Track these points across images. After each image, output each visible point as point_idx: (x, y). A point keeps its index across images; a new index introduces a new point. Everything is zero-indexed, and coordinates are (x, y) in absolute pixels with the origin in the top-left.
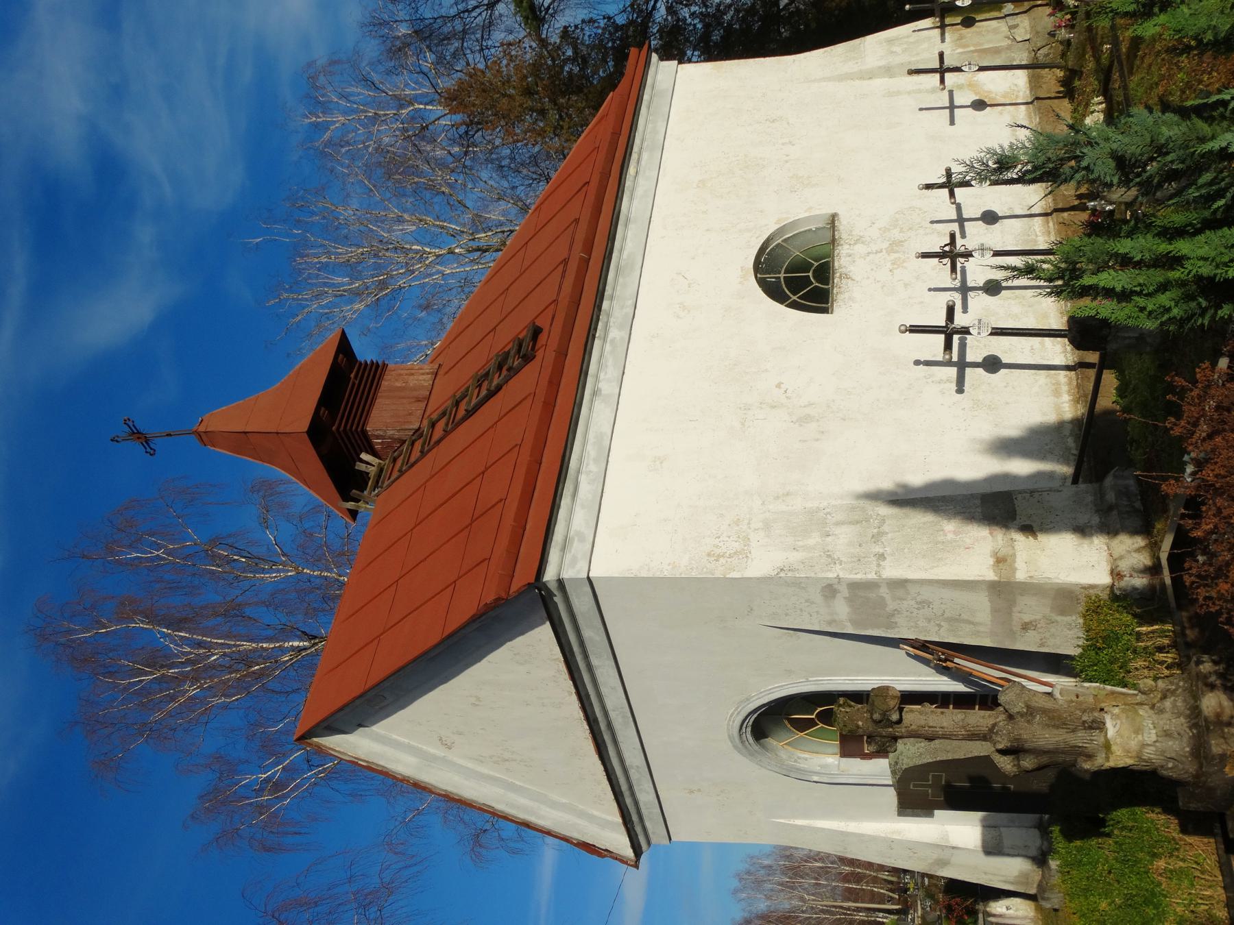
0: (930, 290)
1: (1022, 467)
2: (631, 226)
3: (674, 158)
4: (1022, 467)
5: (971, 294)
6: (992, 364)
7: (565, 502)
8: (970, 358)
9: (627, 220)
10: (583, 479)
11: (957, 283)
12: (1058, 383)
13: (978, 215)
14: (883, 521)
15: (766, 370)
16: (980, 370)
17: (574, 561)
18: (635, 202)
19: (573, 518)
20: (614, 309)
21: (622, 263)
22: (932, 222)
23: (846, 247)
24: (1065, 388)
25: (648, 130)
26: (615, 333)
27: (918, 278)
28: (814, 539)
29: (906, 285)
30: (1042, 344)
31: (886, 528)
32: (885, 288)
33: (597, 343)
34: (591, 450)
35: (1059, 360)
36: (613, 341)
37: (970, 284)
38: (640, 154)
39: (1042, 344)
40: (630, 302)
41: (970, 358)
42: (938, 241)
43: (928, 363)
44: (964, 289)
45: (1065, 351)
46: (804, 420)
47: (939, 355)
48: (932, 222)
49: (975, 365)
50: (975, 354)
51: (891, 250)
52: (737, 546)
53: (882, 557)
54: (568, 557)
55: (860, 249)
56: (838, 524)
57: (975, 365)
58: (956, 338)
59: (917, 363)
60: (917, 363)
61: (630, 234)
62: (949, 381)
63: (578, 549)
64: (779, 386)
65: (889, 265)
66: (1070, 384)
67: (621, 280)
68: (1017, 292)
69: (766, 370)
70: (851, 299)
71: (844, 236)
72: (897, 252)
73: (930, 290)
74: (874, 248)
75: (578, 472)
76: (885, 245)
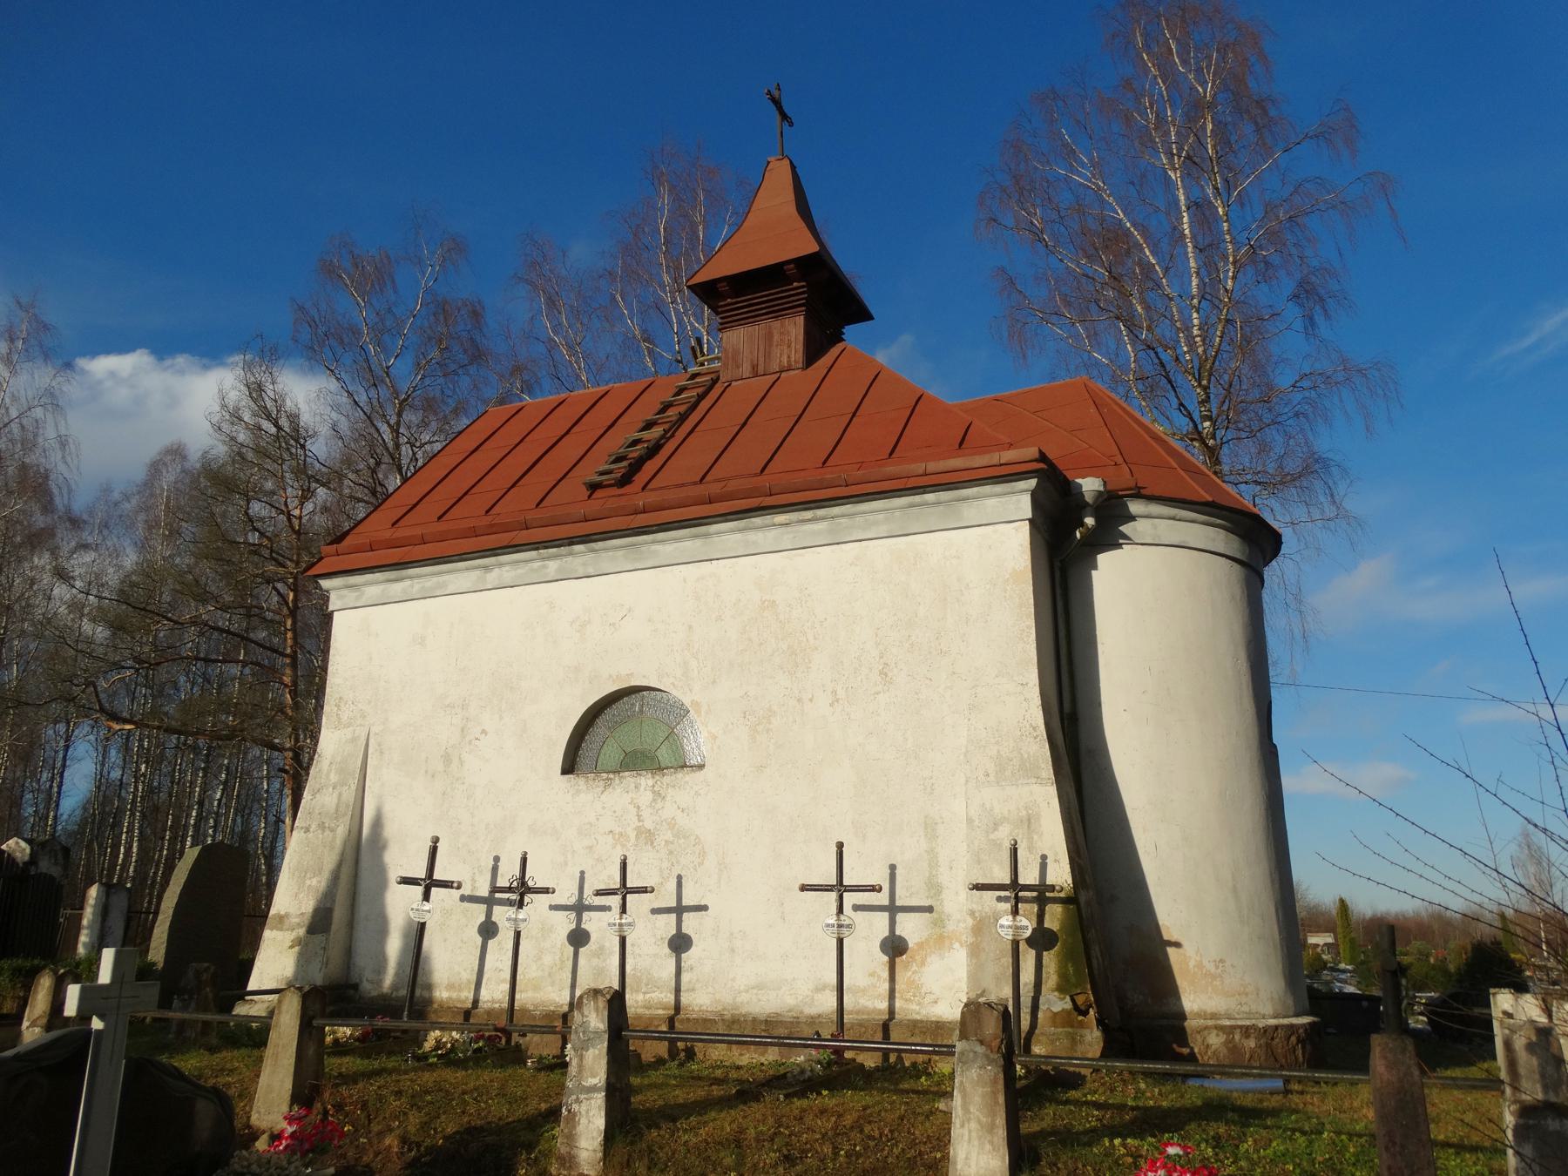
0: (582, 873)
1: (394, 946)
2: (698, 542)
3: (935, 546)
4: (394, 946)
5: (573, 915)
6: (488, 930)
7: (378, 576)
8: (497, 909)
9: (707, 535)
10: (407, 583)
11: (590, 899)
12: (460, 990)
13: (685, 930)
14: (332, 830)
15: (501, 718)
16: (483, 918)
17: (341, 597)
18: (738, 536)
19: (373, 586)
20: (580, 557)
21: (644, 548)
22: (679, 878)
23: (650, 782)
24: (454, 995)
25: (871, 517)
26: (553, 566)
27: (599, 860)
28: (334, 778)
29: (590, 847)
30: (503, 981)
31: (327, 832)
32: (575, 831)
33: (533, 554)
34: (430, 583)
35: (485, 994)
36: (544, 567)
37: (586, 915)
38: (823, 518)
39: (503, 981)
40: (591, 571)
41: (497, 909)
42: (536, 877)
43: (495, 869)
44: (579, 908)
45: (493, 1001)
46: (447, 759)
47: (502, 882)
48: (679, 878)
49: (489, 914)
50: (501, 914)
51: (640, 831)
52: (344, 718)
53: (307, 830)
54: (345, 592)
55: (645, 797)
56: (340, 795)
57: (489, 914)
58: (514, 897)
59: (497, 859)
60: (497, 859)
61: (688, 544)
62: (474, 888)
63: (350, 597)
64: (484, 732)
65: (617, 830)
66: (459, 1001)
67: (621, 553)
68: (570, 964)
69: (501, 718)
70: (578, 792)
71: (666, 779)
72: (637, 837)
73: (582, 873)
74: (646, 813)
75: (411, 578)
76: (648, 824)
